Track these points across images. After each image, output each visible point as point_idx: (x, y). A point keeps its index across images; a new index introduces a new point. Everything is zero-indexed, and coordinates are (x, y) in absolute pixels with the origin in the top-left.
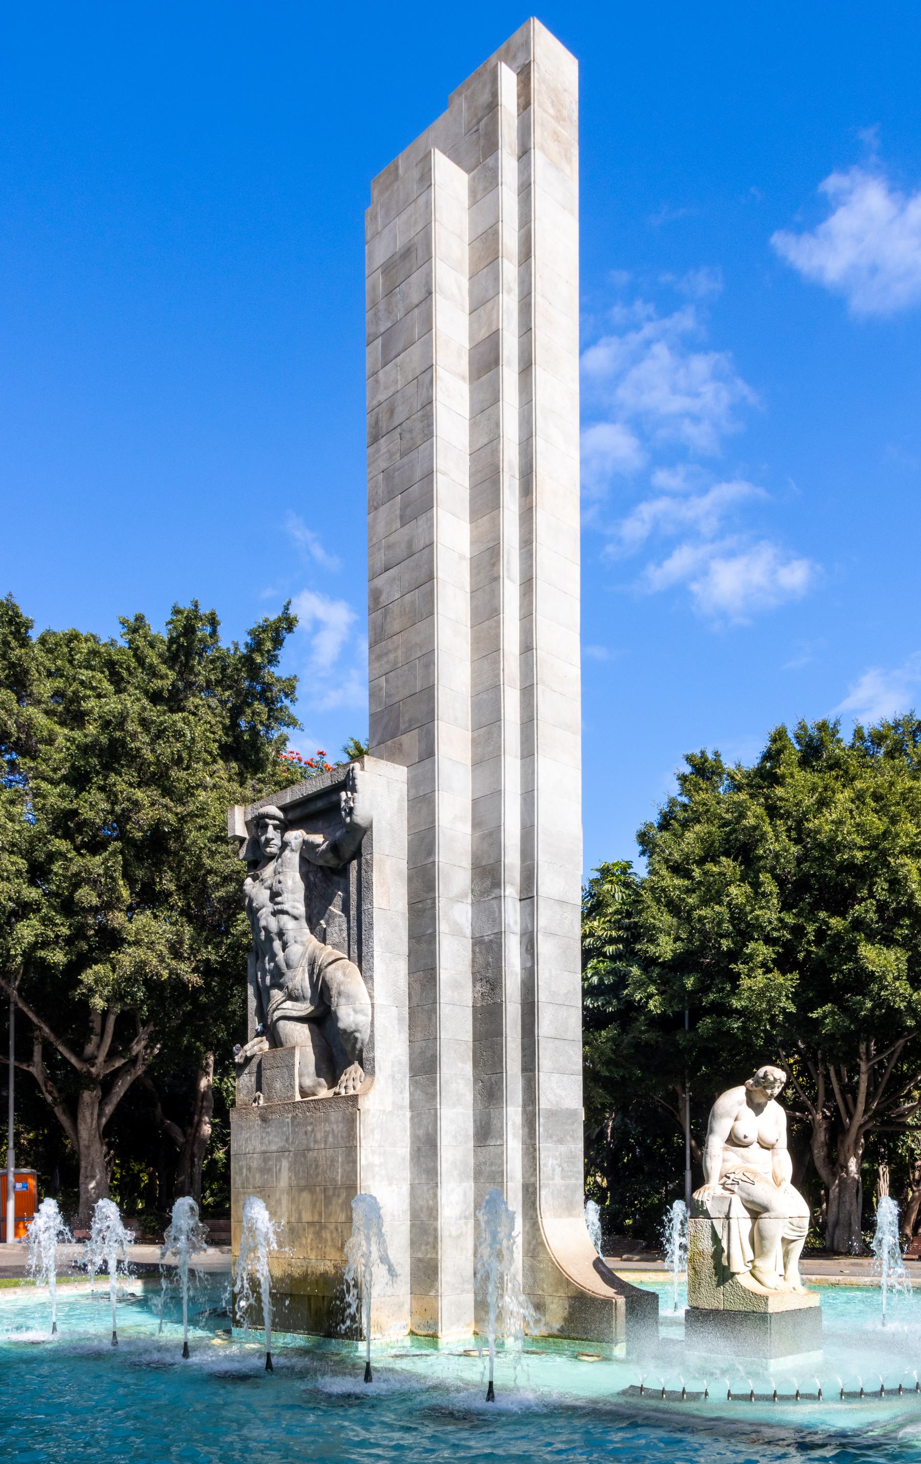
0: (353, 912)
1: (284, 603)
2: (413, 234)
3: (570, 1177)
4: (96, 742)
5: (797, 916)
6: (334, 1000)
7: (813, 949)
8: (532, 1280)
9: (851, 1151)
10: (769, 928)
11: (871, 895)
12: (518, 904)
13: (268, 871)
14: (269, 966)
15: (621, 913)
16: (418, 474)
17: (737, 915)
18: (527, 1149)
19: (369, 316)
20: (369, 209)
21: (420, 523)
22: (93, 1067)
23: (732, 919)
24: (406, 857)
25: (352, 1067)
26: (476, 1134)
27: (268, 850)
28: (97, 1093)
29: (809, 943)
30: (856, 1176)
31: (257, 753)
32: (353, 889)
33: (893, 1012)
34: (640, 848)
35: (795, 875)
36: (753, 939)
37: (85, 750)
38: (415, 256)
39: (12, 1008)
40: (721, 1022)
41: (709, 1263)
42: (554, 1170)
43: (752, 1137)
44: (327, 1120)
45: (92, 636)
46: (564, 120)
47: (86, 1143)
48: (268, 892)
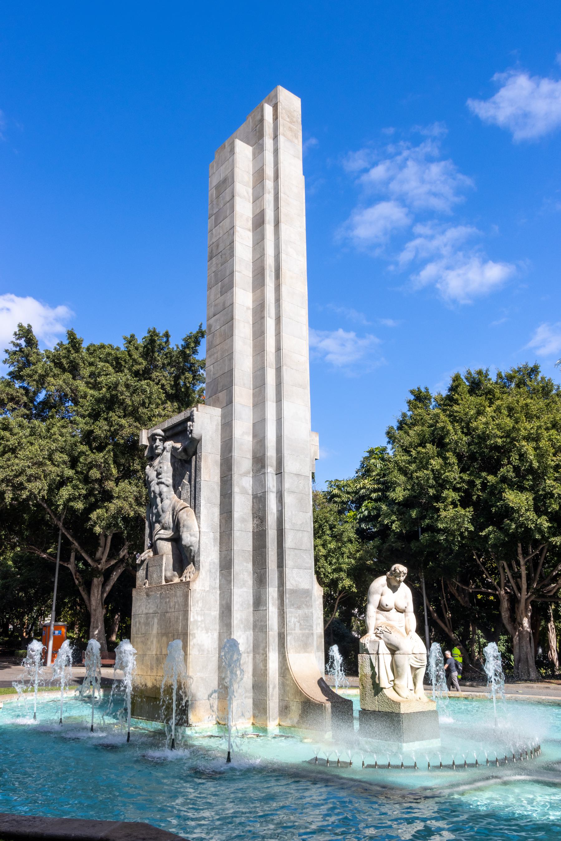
0: (193, 483)
1: (199, 324)
2: (227, 172)
3: (305, 629)
4: (104, 396)
5: (470, 475)
6: (181, 529)
7: (480, 494)
8: (283, 691)
9: (524, 614)
10: (455, 482)
11: (509, 463)
12: (275, 477)
13: (156, 462)
14: (155, 511)
15: (379, 476)
16: (228, 273)
17: (437, 476)
18: (280, 612)
19: (210, 207)
20: (211, 164)
21: (228, 294)
22: (99, 564)
23: (435, 478)
24: (220, 454)
25: (190, 566)
26: (254, 603)
27: (157, 451)
28: (101, 579)
29: (478, 490)
30: (529, 630)
31: (188, 397)
32: (193, 471)
33: (528, 530)
34: (388, 440)
35: (467, 452)
36: (446, 488)
37: (99, 401)
38: (228, 182)
39: (60, 533)
40: (433, 536)
41: (370, 681)
42: (295, 625)
43: (391, 605)
44: (176, 596)
45: (110, 345)
46: (294, 122)
47: (94, 607)
48: (156, 472)
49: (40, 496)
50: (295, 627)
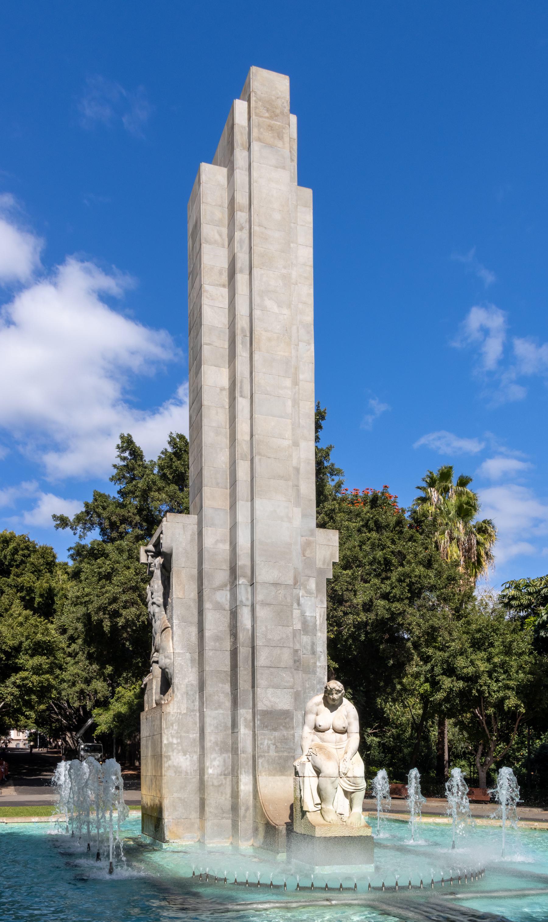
42: (269, 747)
49: (139, 622)
50: (268, 750)
